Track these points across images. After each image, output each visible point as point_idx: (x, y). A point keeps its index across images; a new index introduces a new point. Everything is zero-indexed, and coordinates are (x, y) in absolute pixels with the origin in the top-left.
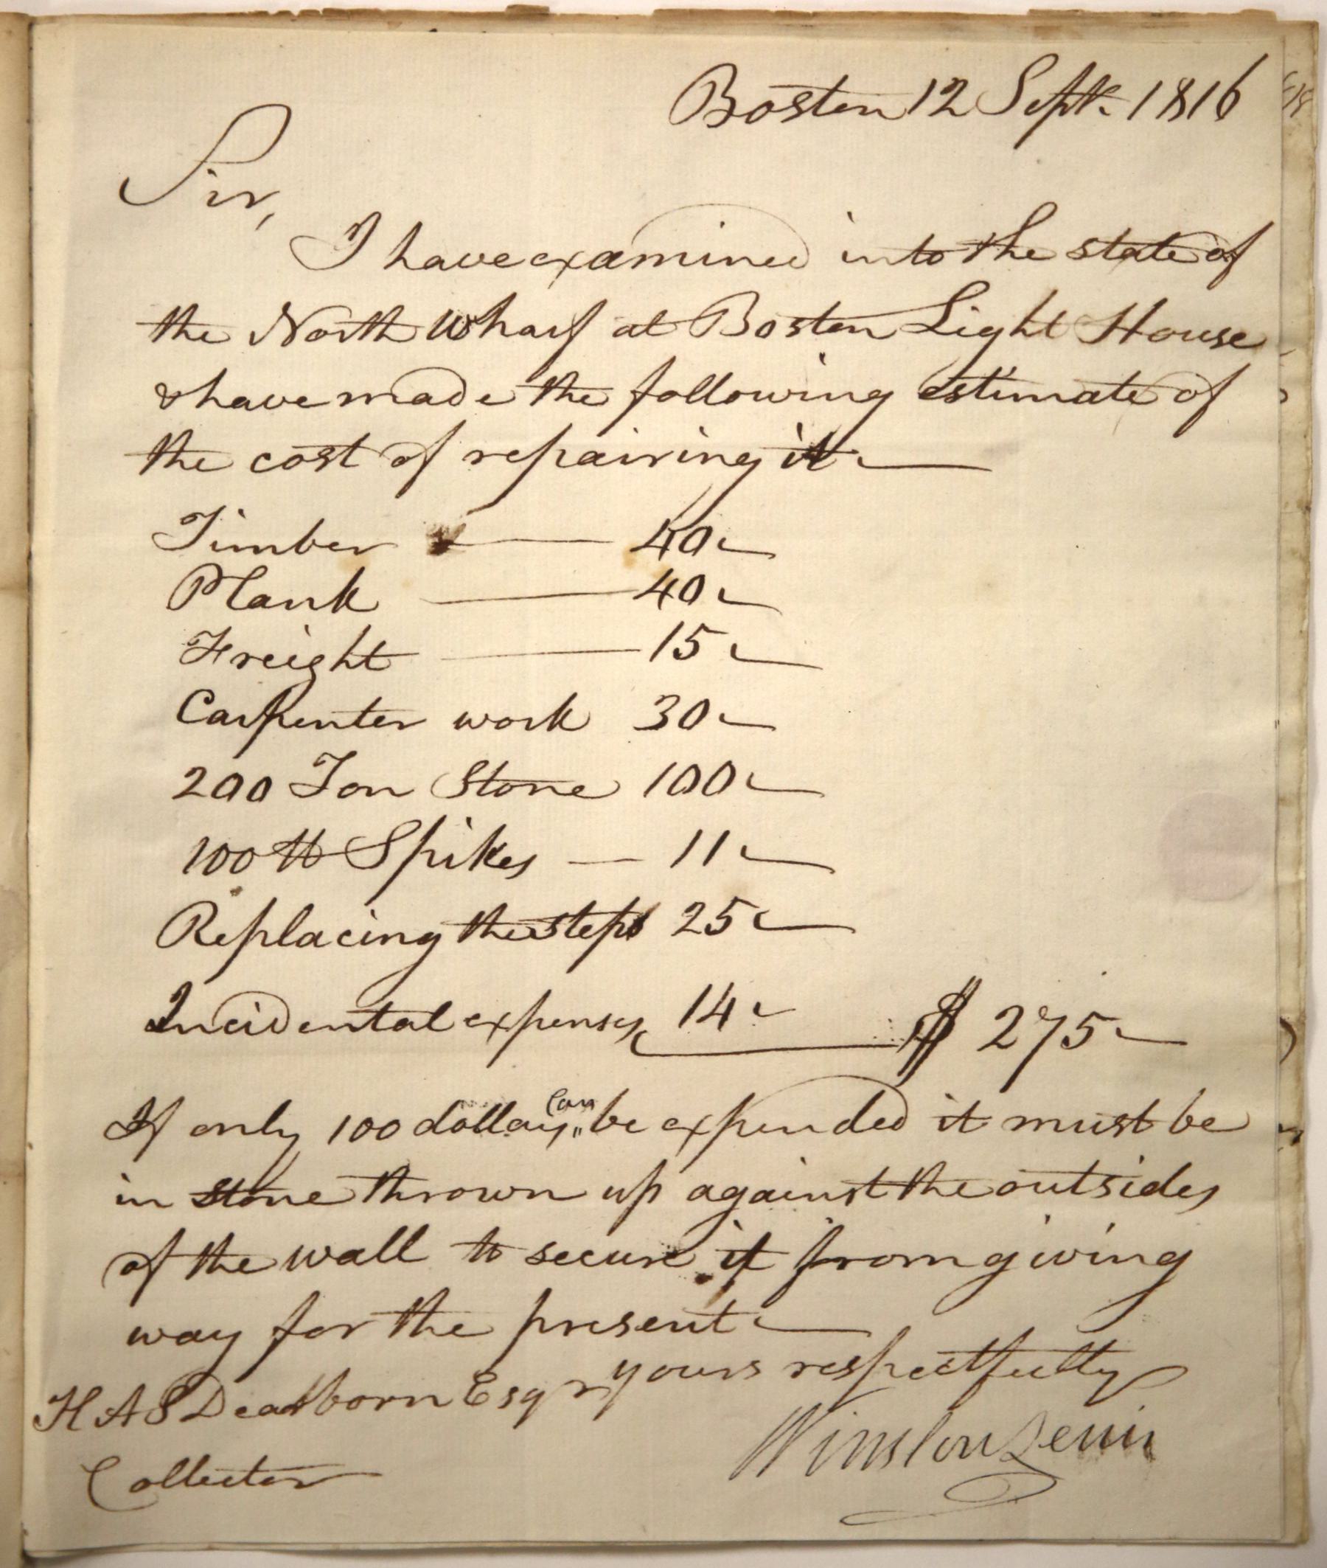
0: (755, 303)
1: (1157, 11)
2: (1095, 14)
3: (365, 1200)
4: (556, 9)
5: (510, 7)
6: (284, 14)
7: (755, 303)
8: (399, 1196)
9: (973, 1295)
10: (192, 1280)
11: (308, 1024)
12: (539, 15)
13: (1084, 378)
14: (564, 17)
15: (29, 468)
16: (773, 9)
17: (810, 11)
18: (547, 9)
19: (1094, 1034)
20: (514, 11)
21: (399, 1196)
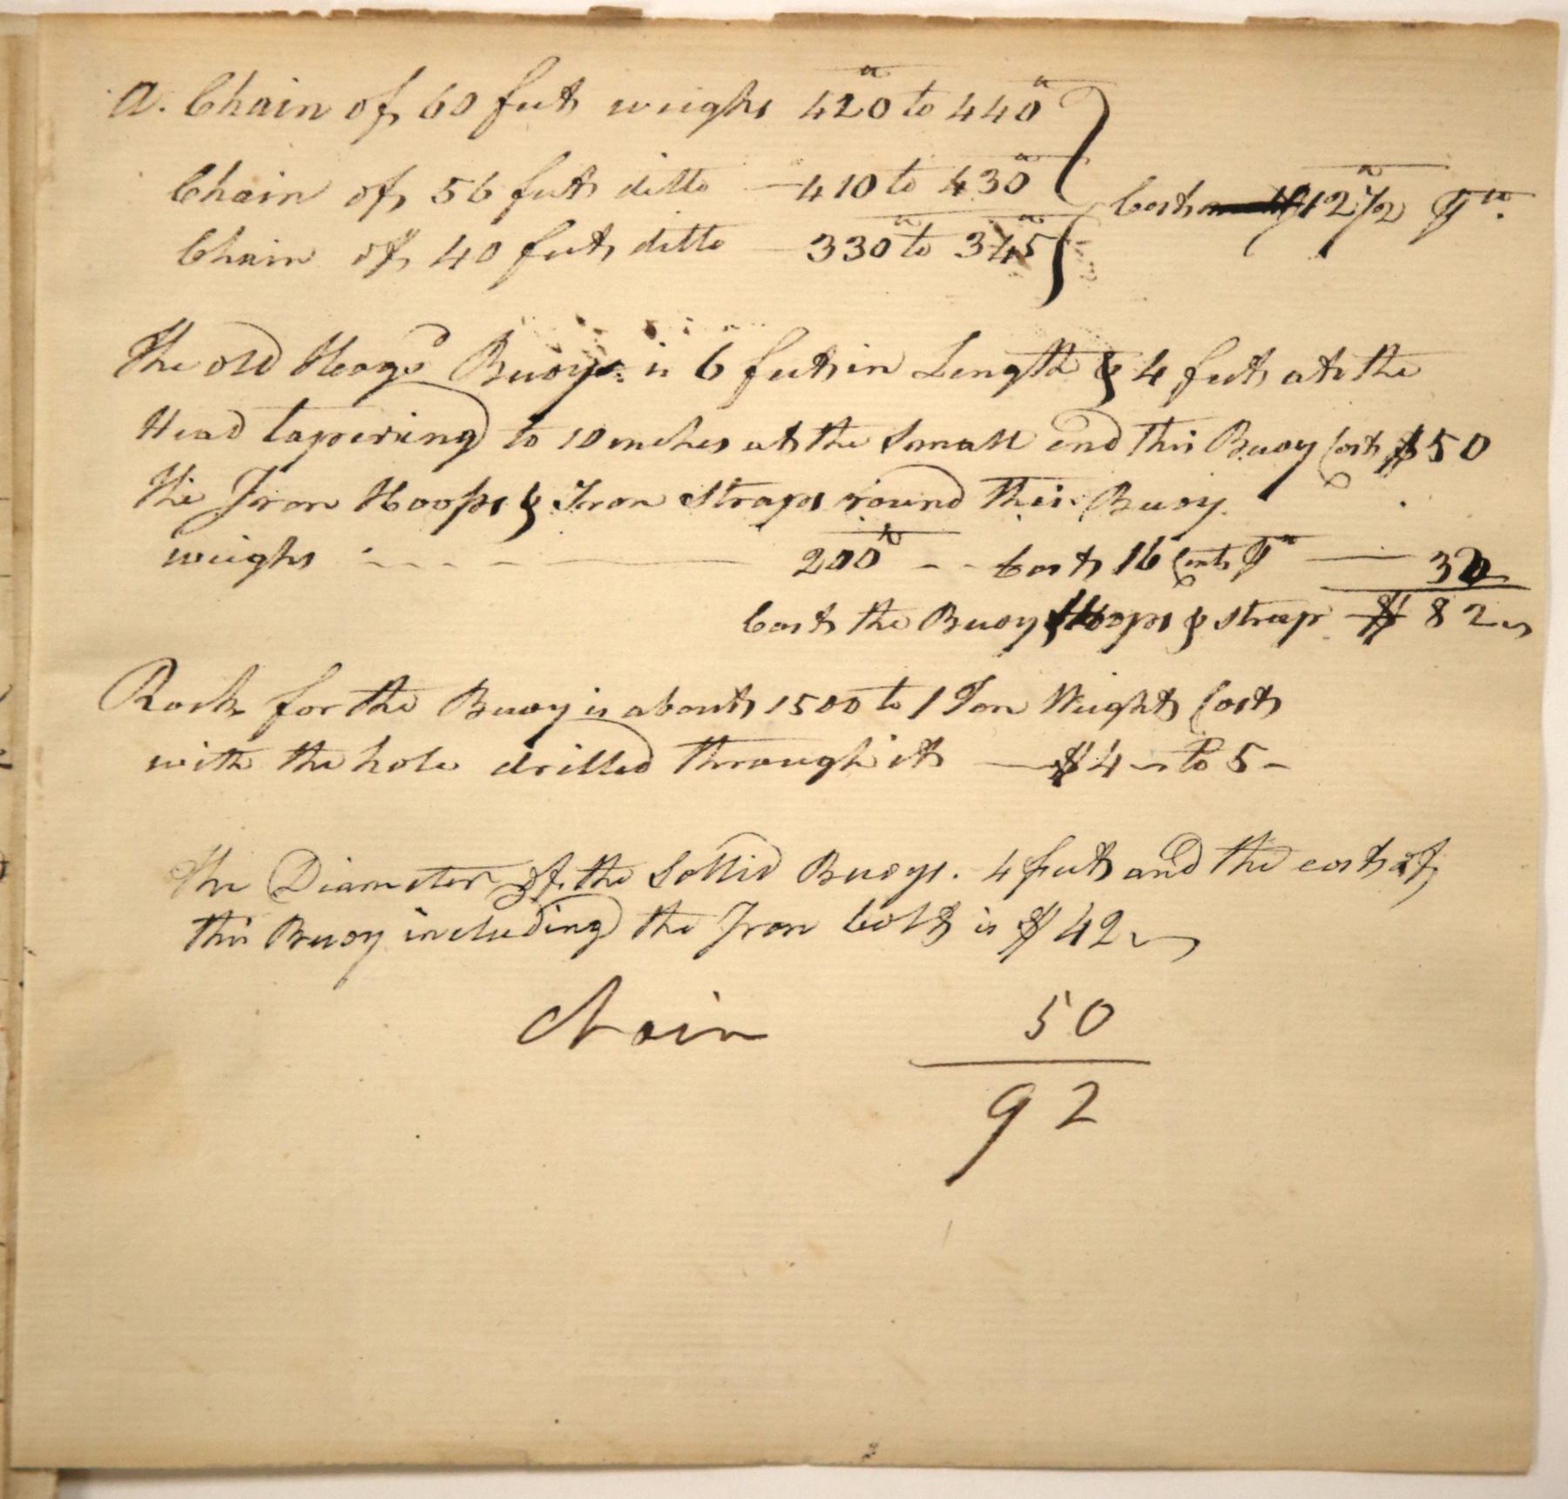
0: (1106, 1019)
1: (1408, 20)
2: (1332, 23)
3: (942, 690)
4: (651, 12)
5: (593, 9)
6: (307, 15)
7: (1106, 1019)
8: (238, 767)
9: (535, 1023)
10: (939, 687)
11: (1064, 685)
12: (630, 18)
13: (1141, 368)
14: (661, 22)
15: (15, 365)
16: (925, 14)
17: (971, 16)
18: (639, 12)
19: (406, 204)
20: (598, 14)
21: (238, 767)
